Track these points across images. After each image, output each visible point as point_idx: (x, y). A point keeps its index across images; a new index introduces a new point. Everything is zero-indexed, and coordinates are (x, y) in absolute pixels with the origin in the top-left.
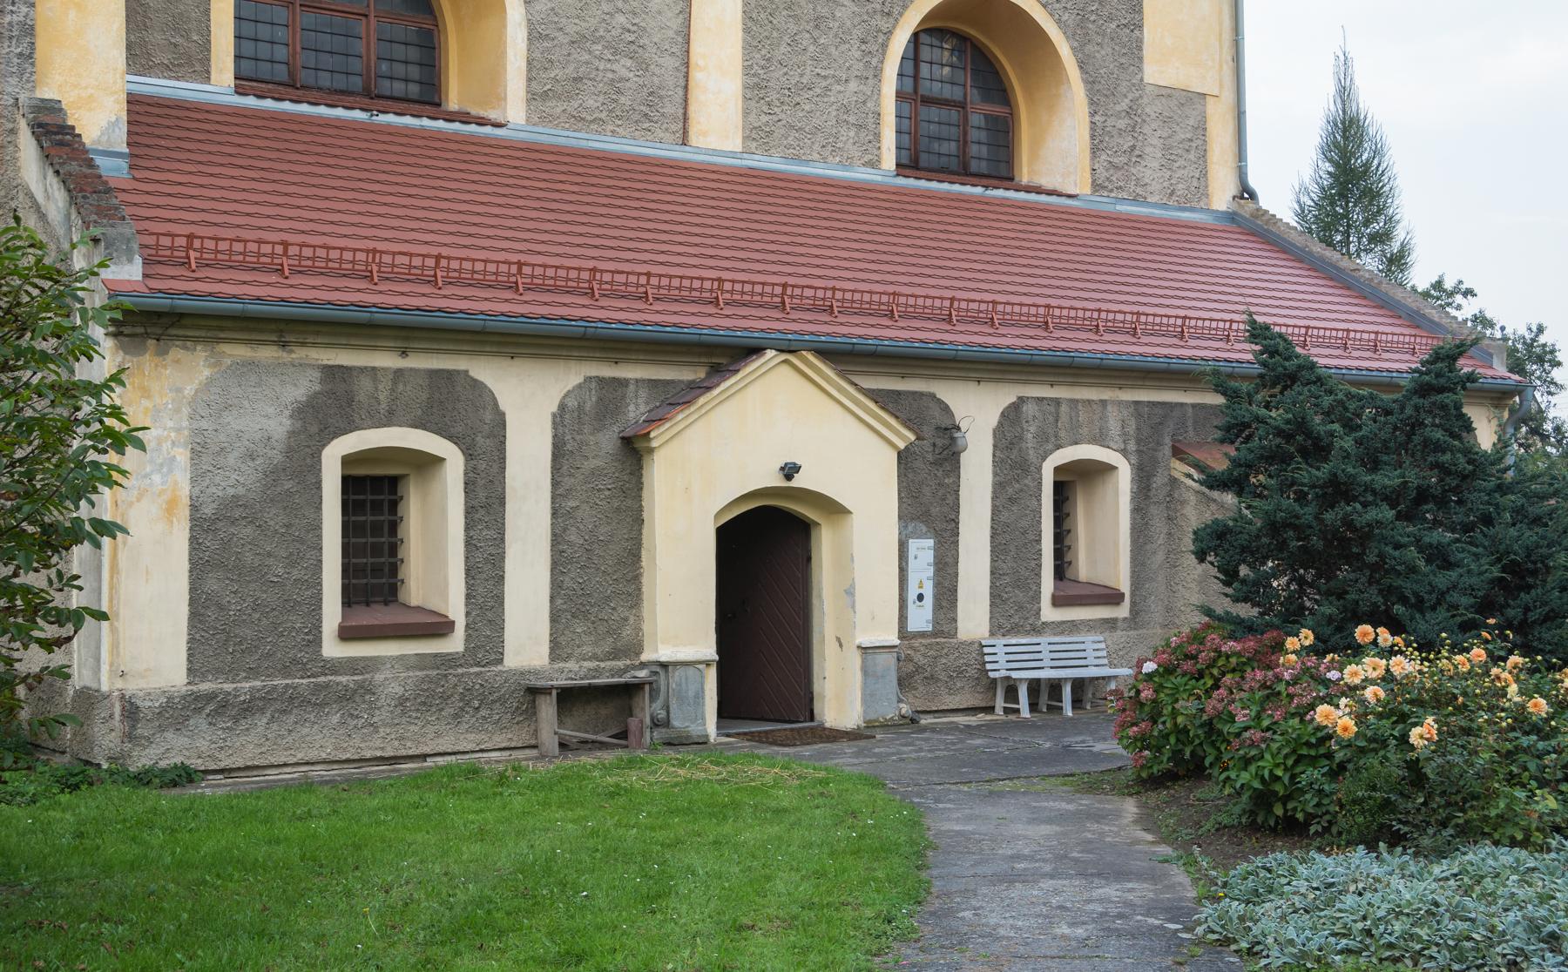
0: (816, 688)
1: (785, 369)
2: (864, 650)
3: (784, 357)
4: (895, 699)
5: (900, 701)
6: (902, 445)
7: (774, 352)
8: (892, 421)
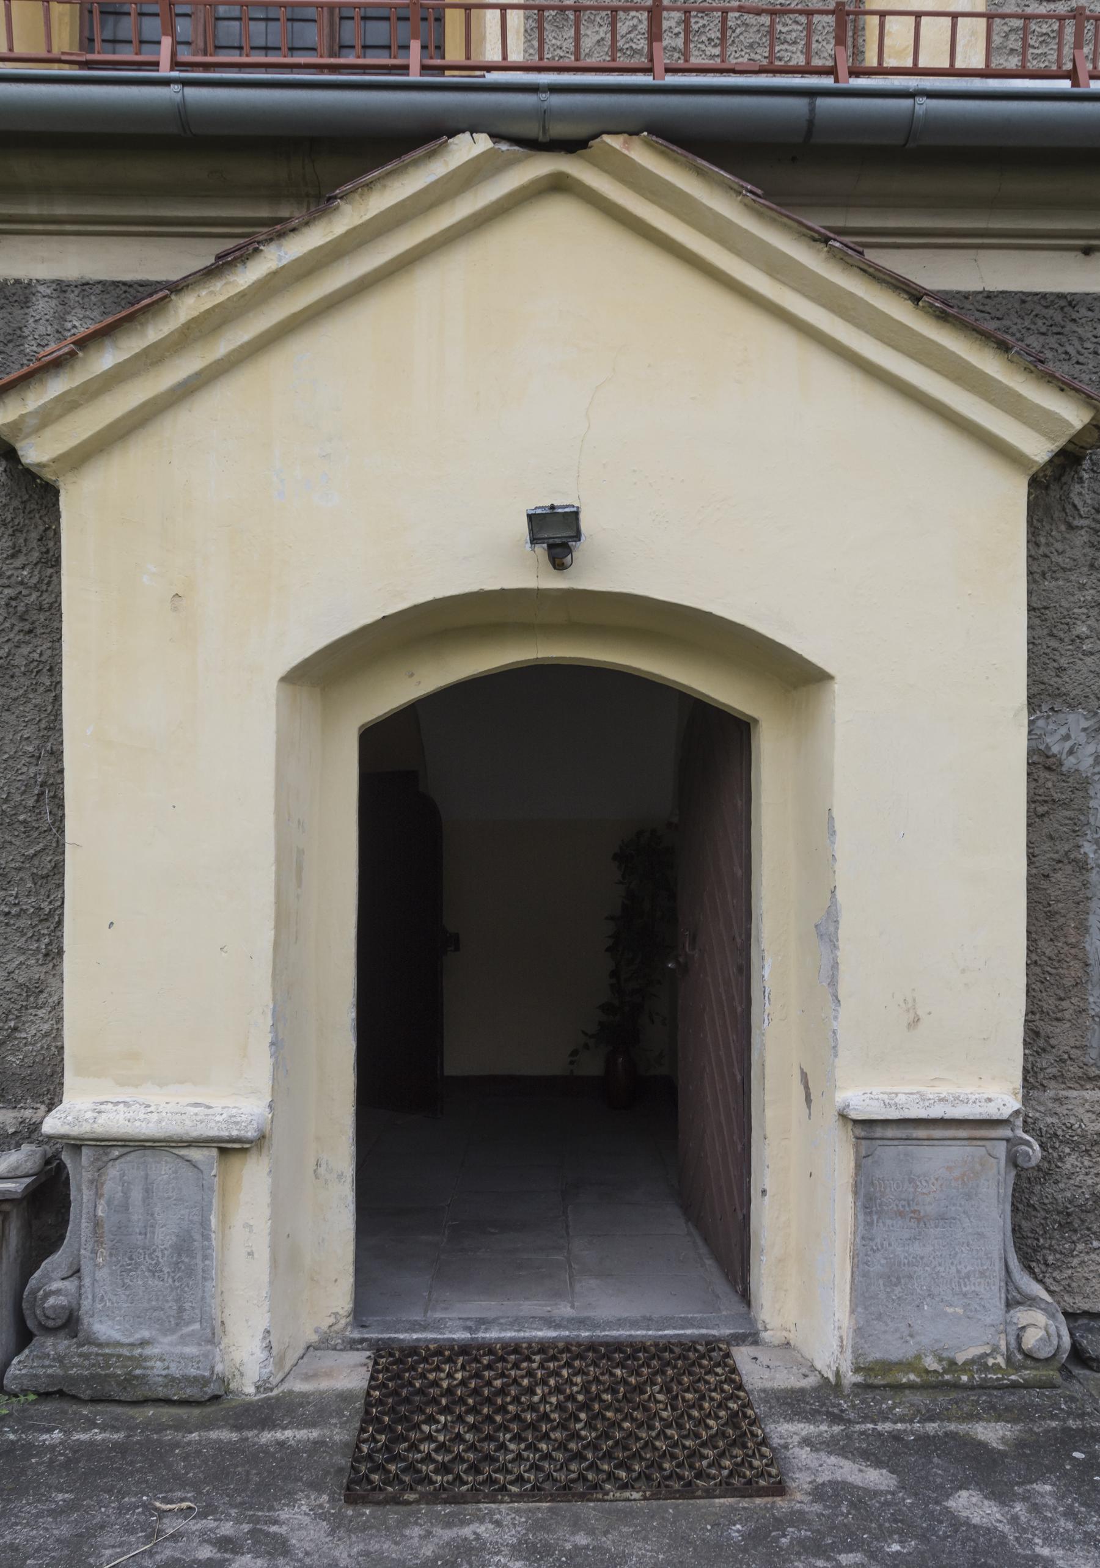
0: (353, 1148)
1: (560, 216)
2: (867, 1130)
3: (542, 166)
4: (994, 1296)
5: (1015, 1300)
6: (1039, 449)
7: (483, 143)
8: (988, 363)
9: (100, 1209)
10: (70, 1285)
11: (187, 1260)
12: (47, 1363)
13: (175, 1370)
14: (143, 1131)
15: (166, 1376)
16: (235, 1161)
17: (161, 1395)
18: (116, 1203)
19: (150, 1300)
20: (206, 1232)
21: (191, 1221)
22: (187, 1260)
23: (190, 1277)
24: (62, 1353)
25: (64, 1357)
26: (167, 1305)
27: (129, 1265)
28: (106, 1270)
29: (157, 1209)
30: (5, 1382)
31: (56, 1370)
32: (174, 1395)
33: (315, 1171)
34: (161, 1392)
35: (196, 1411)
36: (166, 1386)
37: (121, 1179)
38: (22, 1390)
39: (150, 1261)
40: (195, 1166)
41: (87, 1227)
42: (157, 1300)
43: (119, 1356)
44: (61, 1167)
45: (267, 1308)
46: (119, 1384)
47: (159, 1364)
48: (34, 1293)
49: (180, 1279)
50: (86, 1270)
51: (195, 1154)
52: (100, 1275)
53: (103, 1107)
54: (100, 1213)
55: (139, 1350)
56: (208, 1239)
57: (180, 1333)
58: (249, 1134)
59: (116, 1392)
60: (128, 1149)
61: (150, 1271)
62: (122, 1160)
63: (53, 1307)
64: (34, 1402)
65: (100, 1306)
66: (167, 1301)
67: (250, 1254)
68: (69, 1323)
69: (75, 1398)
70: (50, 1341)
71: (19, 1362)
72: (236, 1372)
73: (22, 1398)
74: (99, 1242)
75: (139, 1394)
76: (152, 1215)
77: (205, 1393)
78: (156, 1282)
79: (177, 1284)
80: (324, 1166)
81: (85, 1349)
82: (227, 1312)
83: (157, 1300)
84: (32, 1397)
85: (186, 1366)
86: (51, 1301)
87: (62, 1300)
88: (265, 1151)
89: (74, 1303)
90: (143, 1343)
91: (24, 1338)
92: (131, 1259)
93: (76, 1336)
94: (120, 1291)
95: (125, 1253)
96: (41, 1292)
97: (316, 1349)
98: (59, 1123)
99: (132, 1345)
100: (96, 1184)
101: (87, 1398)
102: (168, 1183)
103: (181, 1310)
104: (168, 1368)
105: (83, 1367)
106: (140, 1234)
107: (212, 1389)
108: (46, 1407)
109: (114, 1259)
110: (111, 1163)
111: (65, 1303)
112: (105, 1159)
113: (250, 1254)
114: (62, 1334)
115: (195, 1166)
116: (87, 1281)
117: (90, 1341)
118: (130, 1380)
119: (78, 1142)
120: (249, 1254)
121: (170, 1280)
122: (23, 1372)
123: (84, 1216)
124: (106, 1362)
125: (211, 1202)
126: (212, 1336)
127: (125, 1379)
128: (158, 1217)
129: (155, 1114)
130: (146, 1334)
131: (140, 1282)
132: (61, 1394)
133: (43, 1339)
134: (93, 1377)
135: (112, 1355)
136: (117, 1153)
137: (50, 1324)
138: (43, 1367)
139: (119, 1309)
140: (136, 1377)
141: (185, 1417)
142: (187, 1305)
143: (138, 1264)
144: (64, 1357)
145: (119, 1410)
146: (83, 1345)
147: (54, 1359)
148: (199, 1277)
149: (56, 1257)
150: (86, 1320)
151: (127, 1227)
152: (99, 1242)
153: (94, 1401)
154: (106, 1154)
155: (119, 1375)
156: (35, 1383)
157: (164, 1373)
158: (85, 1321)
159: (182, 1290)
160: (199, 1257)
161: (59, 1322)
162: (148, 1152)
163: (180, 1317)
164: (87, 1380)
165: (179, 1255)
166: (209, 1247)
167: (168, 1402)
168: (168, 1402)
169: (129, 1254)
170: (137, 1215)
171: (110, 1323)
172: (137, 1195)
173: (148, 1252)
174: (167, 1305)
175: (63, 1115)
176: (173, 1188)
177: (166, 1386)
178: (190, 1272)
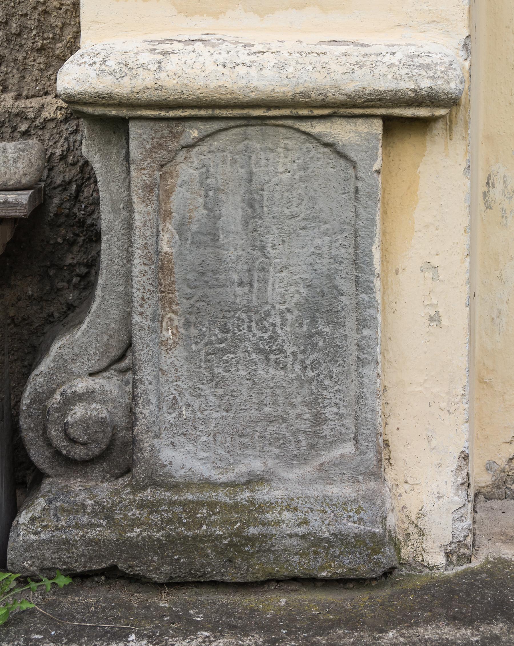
9: (165, 237)
10: (110, 384)
11: (327, 330)
12: (85, 519)
13: (318, 525)
14: (254, 83)
15: (303, 537)
16: (407, 147)
17: (297, 571)
18: (194, 227)
19: (261, 404)
20: (363, 277)
21: (335, 258)
22: (327, 330)
23: (333, 361)
24: (108, 503)
25: (111, 510)
26: (293, 413)
27: (221, 341)
28: (179, 352)
29: (270, 238)
30: (10, 555)
31: (101, 532)
32: (322, 569)
33: (485, 194)
34: (298, 565)
35: (362, 597)
36: (305, 554)
37: (202, 183)
38: (43, 570)
39: (259, 334)
40: (342, 155)
41: (143, 273)
42: (275, 403)
43: (212, 505)
44: (86, 175)
45: (464, 416)
46: (220, 553)
47: (287, 515)
48: (41, 398)
49: (315, 365)
50: (143, 349)
51: (343, 132)
52: (167, 363)
53: (167, 47)
54: (165, 248)
55: (247, 494)
56: (369, 289)
57: (317, 462)
58: (453, 85)
59: (214, 568)
60: (216, 126)
61: (260, 351)
62: (204, 147)
63: (84, 422)
64: (67, 590)
65: (170, 417)
66: (293, 406)
67: (435, 318)
68: (115, 452)
69: (137, 581)
70: (76, 485)
71: (33, 520)
72: (412, 529)
73: (47, 583)
74: (166, 301)
75: (257, 570)
76: (263, 248)
77: (377, 564)
78: (272, 371)
79: (310, 373)
80: (499, 187)
81: (148, 494)
82: (393, 422)
83: (275, 403)
84: (63, 581)
85: (338, 518)
86: (79, 411)
87: (97, 410)
88: (458, 129)
89: (120, 418)
90: (253, 481)
91: (25, 479)
92: (224, 330)
93: (128, 471)
94: (206, 390)
95: (214, 320)
96: (57, 396)
97: (488, 498)
98: (92, 73)
99: (232, 485)
100: (158, 192)
101: (162, 579)
102: (291, 188)
103: (319, 419)
104: (306, 522)
105: (151, 526)
106: (241, 284)
107: (386, 557)
108: (91, 598)
109: (193, 331)
110: (182, 154)
111: (104, 414)
112: (173, 145)
113: (435, 318)
114: (97, 471)
115: (342, 155)
116: (146, 373)
117: (158, 479)
118: (239, 545)
119: (125, 113)
120: (432, 319)
121: (297, 367)
122: (43, 536)
123: (137, 253)
124: (193, 516)
125: (373, 221)
126: (376, 461)
127: (231, 544)
128: (273, 253)
129: (268, 55)
130: (256, 465)
131: (242, 373)
132: (112, 574)
133: (61, 482)
134: (172, 541)
135: (199, 504)
136: (195, 134)
137: (78, 452)
138: (78, 526)
139: (206, 421)
140: (251, 540)
141: (348, 606)
142: (330, 412)
143: (238, 340)
144: (111, 510)
145: (223, 598)
146: (144, 488)
147: (95, 514)
148: (351, 359)
149: (80, 334)
150: (147, 442)
151: (214, 272)
152: (166, 301)
153: (174, 584)
154: (176, 136)
155: (219, 538)
156: (65, 555)
157: (302, 530)
158: (146, 445)
159: (320, 384)
160: (351, 323)
161: (96, 450)
162: (252, 131)
163: (317, 434)
164: (151, 545)
165: (314, 321)
166: (370, 305)
167: (310, 581)
168: (310, 581)
169: (220, 322)
170: (234, 248)
171: (190, 447)
172: (232, 212)
173: (255, 317)
174: (293, 413)
175: (98, 59)
176: (301, 198)
177: (305, 554)
178: (334, 352)
